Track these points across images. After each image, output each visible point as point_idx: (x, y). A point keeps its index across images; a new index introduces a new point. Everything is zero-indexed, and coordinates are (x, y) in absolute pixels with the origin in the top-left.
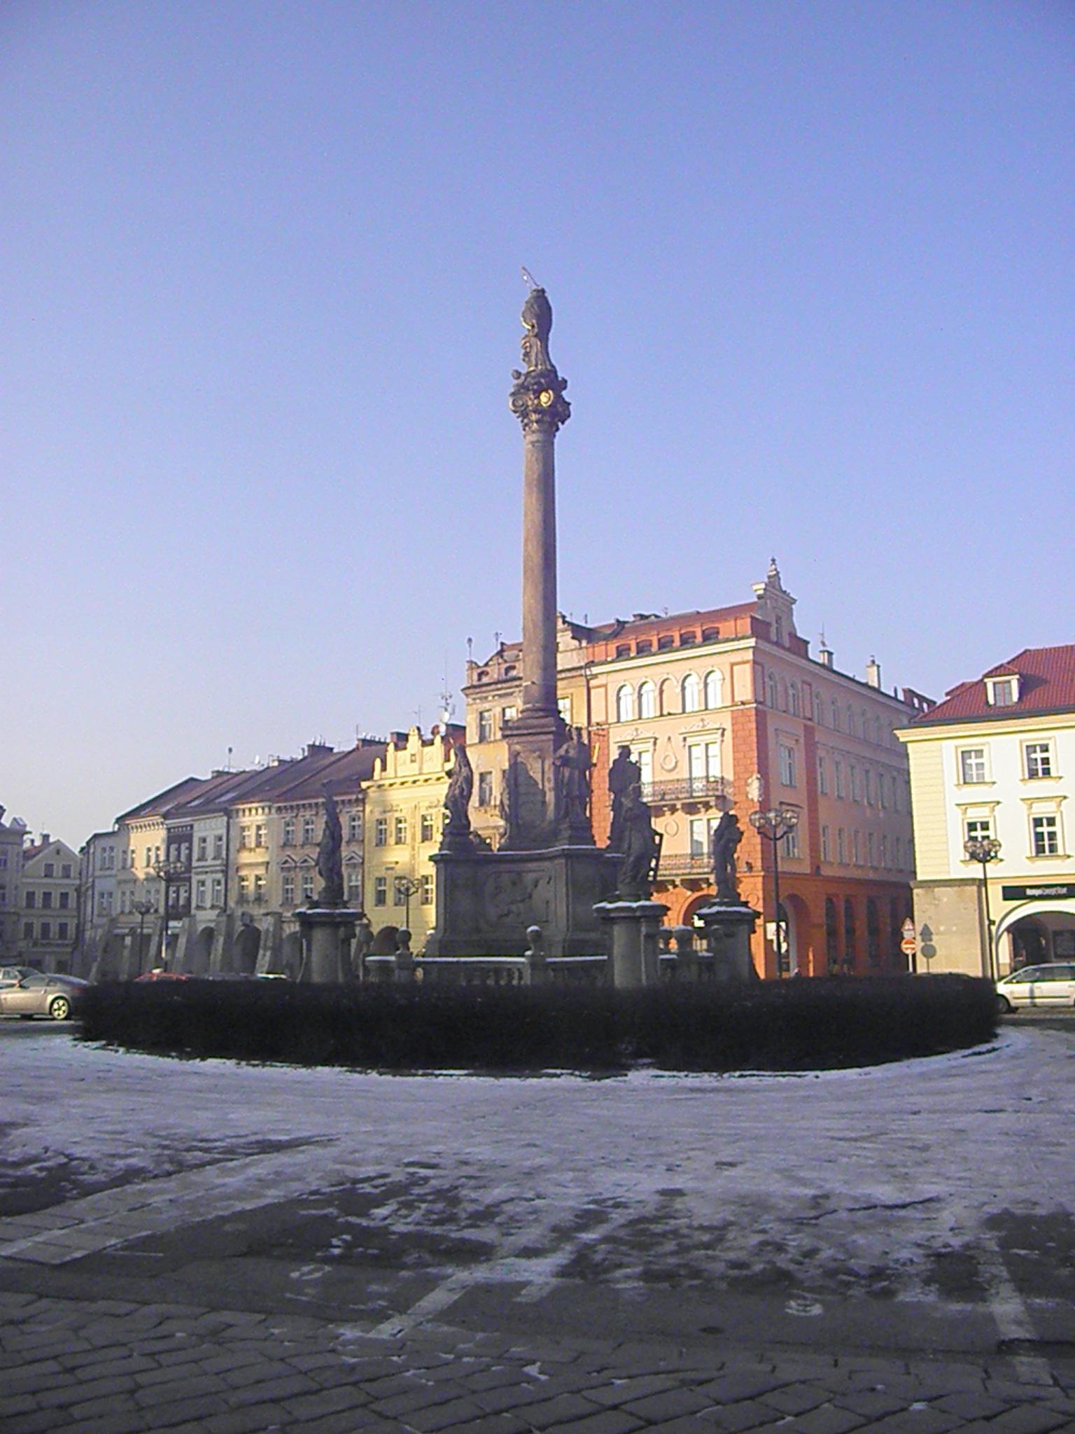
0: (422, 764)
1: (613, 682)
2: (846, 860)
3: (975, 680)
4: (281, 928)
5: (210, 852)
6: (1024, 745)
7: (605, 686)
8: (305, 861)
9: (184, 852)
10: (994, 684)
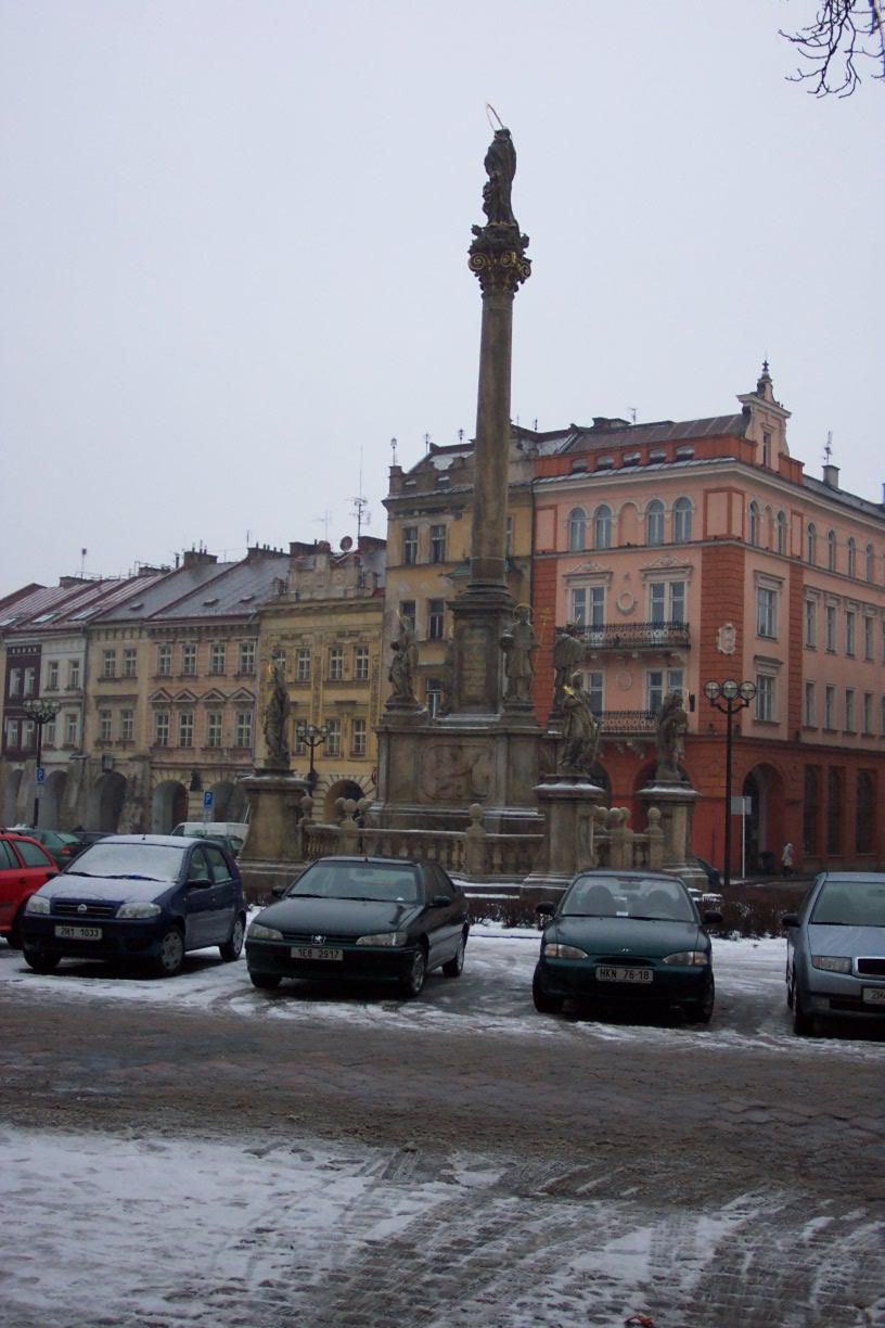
2: (834, 726)
4: (152, 776)
5: (63, 682)
7: (554, 507)
8: (184, 696)
9: (28, 678)
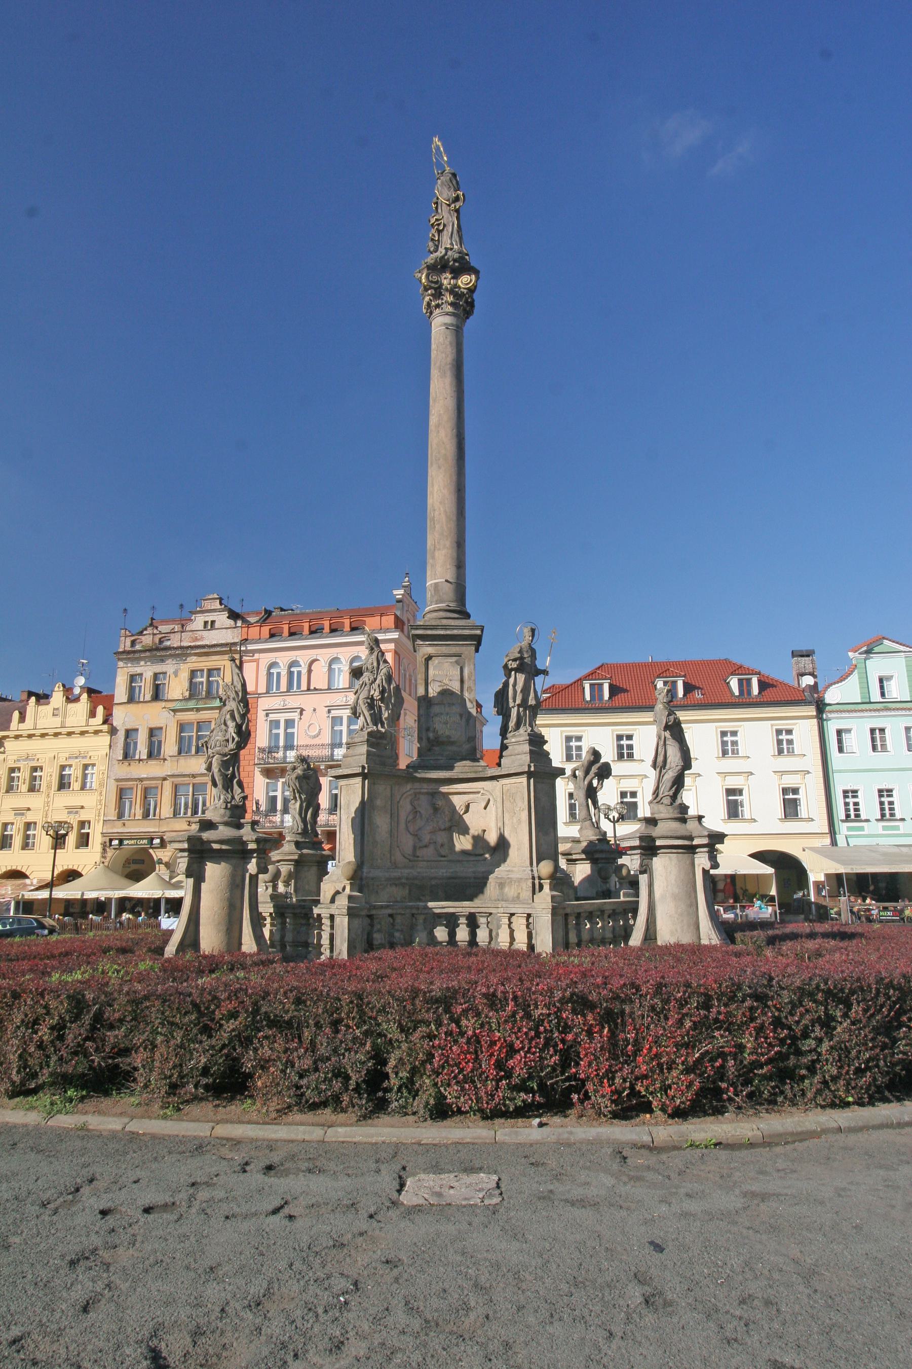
0: (65, 717)
1: (265, 659)
3: (569, 681)
6: (719, 730)
7: (257, 661)
10: (591, 685)
